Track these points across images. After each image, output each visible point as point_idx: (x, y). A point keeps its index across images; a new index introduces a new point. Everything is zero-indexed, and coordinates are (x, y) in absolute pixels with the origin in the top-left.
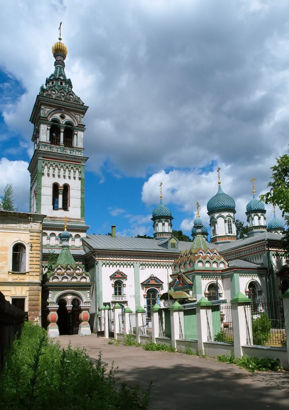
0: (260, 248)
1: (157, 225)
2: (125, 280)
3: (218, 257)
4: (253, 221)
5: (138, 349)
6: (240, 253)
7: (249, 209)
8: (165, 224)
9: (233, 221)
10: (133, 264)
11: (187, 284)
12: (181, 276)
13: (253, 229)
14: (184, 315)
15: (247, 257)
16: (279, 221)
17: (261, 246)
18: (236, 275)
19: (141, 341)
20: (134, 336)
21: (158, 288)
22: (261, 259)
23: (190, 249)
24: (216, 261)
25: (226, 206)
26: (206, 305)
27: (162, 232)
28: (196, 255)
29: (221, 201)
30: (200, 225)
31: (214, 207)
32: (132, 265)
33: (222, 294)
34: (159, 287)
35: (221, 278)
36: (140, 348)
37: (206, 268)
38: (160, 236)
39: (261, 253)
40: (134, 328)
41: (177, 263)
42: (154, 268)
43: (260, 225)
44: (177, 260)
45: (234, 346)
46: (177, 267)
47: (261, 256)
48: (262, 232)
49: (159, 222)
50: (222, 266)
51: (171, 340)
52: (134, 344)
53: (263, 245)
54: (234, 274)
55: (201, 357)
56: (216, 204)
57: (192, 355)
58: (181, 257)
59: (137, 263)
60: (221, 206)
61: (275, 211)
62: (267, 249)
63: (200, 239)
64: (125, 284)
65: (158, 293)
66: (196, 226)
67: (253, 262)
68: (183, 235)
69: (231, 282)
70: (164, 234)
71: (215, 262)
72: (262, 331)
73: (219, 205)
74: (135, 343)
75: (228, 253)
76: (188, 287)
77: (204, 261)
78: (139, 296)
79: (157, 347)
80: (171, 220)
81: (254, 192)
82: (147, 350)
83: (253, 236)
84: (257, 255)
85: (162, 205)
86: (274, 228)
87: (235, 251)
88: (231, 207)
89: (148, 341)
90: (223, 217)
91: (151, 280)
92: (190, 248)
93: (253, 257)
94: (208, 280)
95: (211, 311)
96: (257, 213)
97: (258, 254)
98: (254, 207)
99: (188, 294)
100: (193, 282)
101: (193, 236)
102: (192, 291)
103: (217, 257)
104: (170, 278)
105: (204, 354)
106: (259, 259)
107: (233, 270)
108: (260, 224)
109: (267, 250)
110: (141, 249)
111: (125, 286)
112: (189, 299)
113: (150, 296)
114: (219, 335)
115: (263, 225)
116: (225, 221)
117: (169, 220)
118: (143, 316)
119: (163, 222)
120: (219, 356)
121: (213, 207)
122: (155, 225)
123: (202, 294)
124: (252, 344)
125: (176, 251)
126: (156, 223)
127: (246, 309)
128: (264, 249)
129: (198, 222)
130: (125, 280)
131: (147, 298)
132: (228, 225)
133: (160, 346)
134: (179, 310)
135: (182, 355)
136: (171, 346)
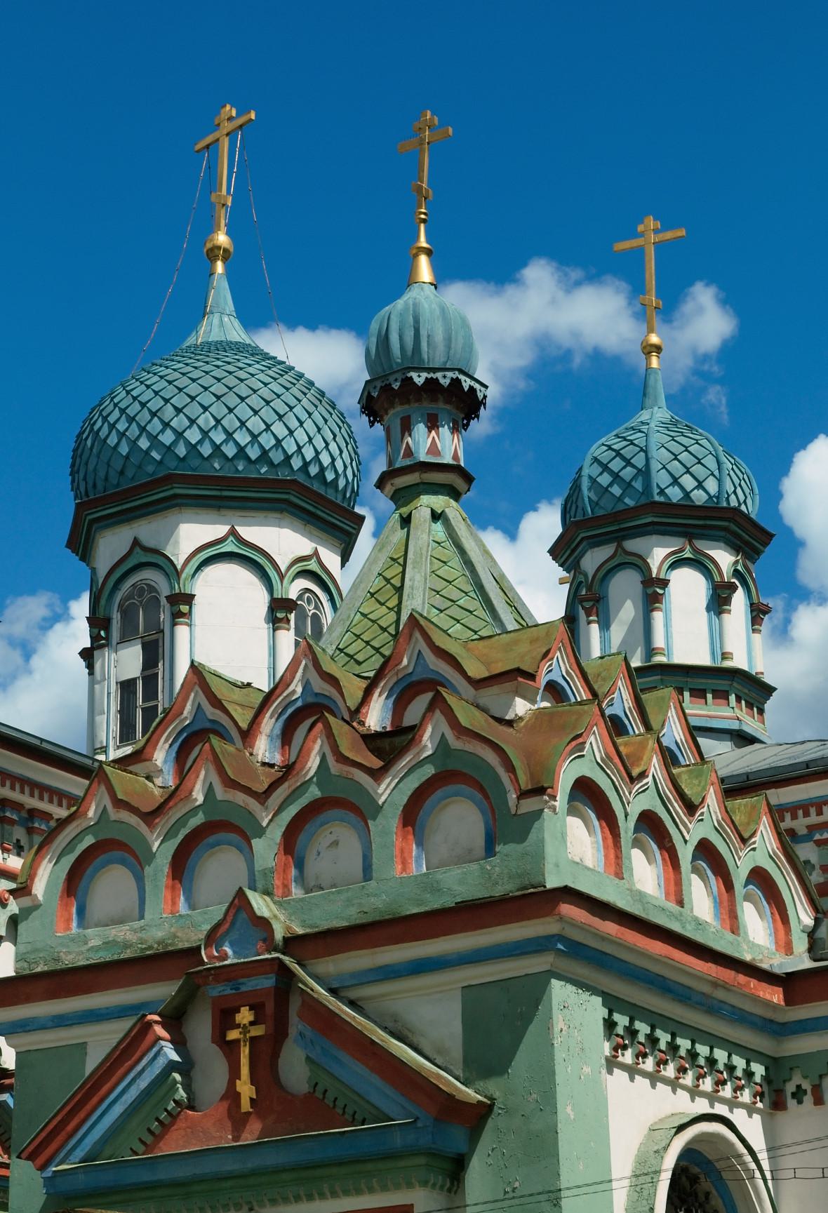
4: (658, 617)
25: (296, 463)
31: (181, 451)
43: (728, 664)
56: (206, 420)
60: (253, 453)
73: (229, 435)
81: (658, 349)
94: (654, 1078)
96: (699, 544)
98: (675, 481)
108: (725, 656)
116: (279, 610)
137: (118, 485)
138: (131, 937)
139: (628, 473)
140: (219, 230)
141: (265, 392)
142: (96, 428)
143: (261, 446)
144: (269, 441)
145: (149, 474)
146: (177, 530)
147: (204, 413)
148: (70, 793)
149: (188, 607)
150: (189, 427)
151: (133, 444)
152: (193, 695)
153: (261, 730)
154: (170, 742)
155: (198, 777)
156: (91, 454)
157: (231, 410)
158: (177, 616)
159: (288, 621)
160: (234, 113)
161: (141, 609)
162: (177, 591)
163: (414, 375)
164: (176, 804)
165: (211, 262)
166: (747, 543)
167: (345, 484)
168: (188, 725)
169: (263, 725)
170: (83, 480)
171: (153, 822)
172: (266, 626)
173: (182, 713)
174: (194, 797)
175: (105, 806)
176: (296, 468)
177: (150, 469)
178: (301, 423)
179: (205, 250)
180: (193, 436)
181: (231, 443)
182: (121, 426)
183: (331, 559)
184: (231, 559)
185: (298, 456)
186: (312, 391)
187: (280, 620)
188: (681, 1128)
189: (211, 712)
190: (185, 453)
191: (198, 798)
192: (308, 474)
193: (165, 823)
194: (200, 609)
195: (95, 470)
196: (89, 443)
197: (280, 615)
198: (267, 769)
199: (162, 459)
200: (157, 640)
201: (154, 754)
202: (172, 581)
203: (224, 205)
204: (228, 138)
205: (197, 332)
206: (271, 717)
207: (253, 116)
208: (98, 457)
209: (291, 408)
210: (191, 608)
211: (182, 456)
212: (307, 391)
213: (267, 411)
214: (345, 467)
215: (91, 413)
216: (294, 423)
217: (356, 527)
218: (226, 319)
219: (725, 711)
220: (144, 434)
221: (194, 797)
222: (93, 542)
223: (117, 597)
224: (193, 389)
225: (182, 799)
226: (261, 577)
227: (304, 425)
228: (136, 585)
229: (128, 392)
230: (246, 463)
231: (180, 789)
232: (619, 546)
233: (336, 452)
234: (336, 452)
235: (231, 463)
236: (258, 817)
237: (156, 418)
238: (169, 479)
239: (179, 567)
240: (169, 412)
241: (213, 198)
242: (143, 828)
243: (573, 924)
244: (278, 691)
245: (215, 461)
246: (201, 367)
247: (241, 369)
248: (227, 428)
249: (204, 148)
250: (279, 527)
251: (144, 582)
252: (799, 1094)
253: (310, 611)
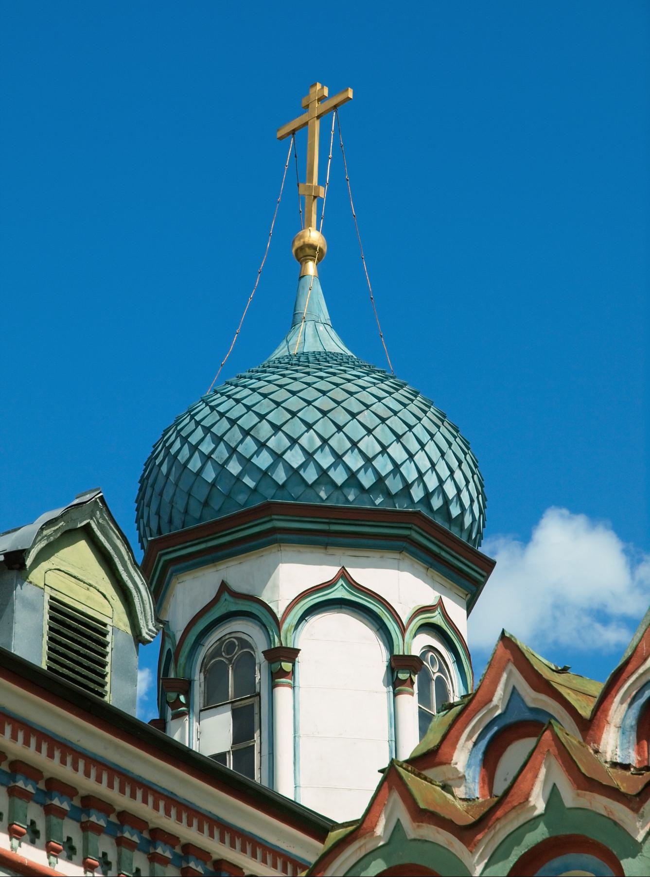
25: (417, 493)
31: (280, 476)
56: (310, 440)
73: (339, 458)
137: (201, 519)
140: (310, 226)
141: (378, 408)
142: (173, 451)
144: (385, 466)
145: (240, 505)
146: (276, 571)
147: (307, 431)
148: (266, 842)
149: (291, 664)
150: (290, 448)
151: (220, 469)
152: (505, 676)
153: (609, 719)
154: (474, 739)
155: (536, 776)
156: (166, 482)
157: (340, 428)
158: (277, 676)
159: (412, 683)
160: (326, 92)
161: (230, 668)
162: (277, 645)
164: (506, 814)
165: (301, 264)
167: (471, 522)
168: (499, 715)
169: (611, 712)
170: (156, 514)
171: (472, 840)
172: (385, 689)
173: (491, 700)
174: (532, 804)
175: (398, 820)
176: (416, 499)
177: (241, 498)
178: (423, 446)
179: (293, 250)
180: (295, 458)
181: (340, 468)
183: (456, 611)
184: (341, 608)
185: (418, 486)
186: (432, 409)
187: (403, 682)
189: (532, 698)
190: (285, 479)
191: (538, 805)
192: (429, 507)
193: (489, 841)
194: (304, 665)
195: (172, 502)
196: (164, 469)
197: (403, 676)
198: (620, 772)
199: (256, 486)
200: (252, 706)
201: (452, 756)
202: (271, 633)
203: (315, 197)
204: (319, 120)
205: (287, 342)
206: (622, 702)
207: (350, 94)
208: (176, 485)
209: (410, 427)
210: (294, 665)
211: (281, 483)
212: (427, 409)
213: (383, 430)
214: (472, 501)
215: (164, 436)
216: (414, 446)
217: (485, 574)
218: (321, 328)
220: (235, 456)
221: (532, 804)
222: (167, 588)
223: (199, 654)
224: (294, 403)
225: (514, 808)
226: (378, 630)
227: (426, 448)
228: (224, 639)
229: (213, 408)
230: (358, 493)
231: (510, 794)
233: (462, 483)
234: (462, 483)
235: (340, 492)
236: (629, 830)
237: (249, 437)
238: (267, 509)
239: (279, 616)
240: (265, 430)
241: (302, 190)
242: (457, 847)
244: (630, 667)
245: (321, 489)
246: (301, 378)
247: (349, 381)
248: (336, 450)
249: (288, 134)
250: (398, 570)
251: (233, 635)
253: (434, 673)
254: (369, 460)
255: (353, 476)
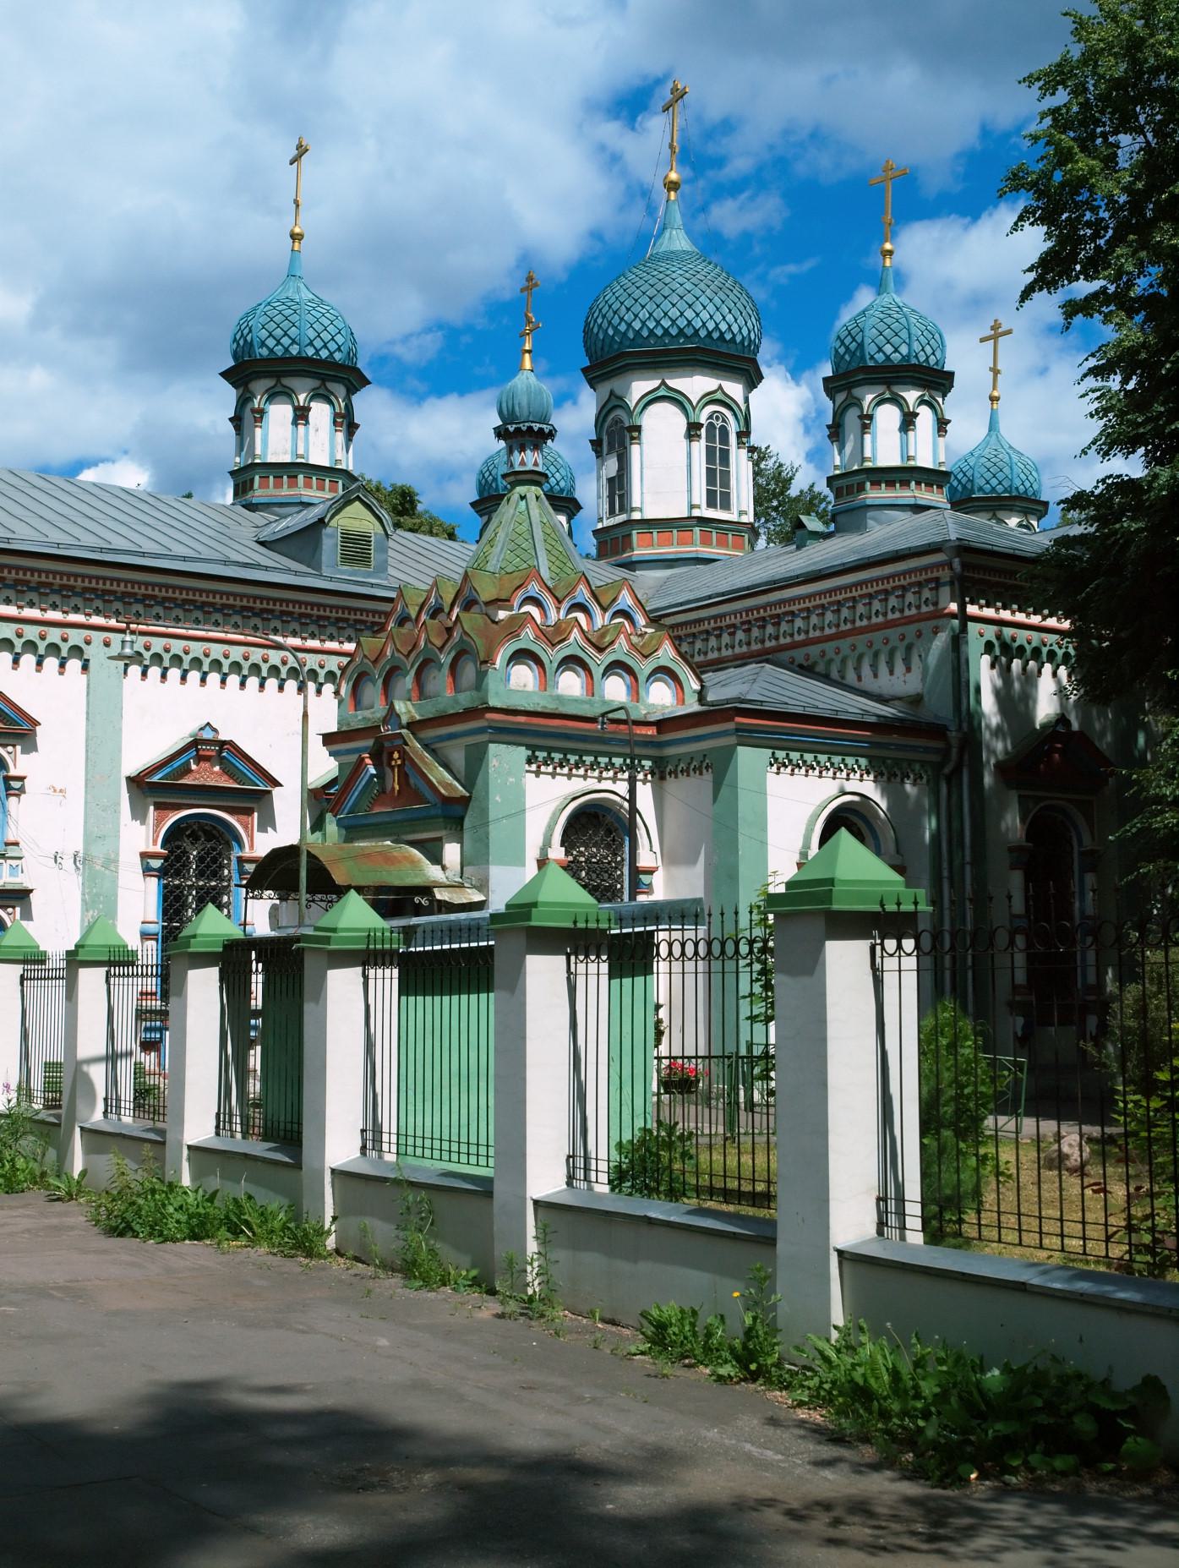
0: (910, 597)
1: (260, 414)
2: (19, 748)
3: (642, 635)
4: (867, 438)
5: (55, 1221)
6: (777, 620)
7: (847, 357)
8: (309, 409)
9: (739, 435)
10: (83, 646)
11: (428, 794)
12: (399, 742)
13: (861, 488)
14: (405, 989)
15: (823, 653)
16: (1015, 458)
17: (919, 584)
18: (749, 759)
19: (85, 1162)
20: (43, 1122)
21: (243, 818)
22: (909, 669)
23: (466, 577)
24: (630, 662)
25: (703, 333)
26: (570, 925)
27: (288, 460)
28: (502, 615)
29: (675, 298)
30: (536, 427)
32: (77, 651)
33: (650, 872)
34: (248, 812)
35: (653, 774)
36: (76, 1216)
37: (560, 699)
38: (271, 490)
39: (911, 630)
40: (49, 1066)
41: (375, 662)
42: (223, 682)
43: (912, 463)
44: (371, 643)
45: (780, 1245)
46: (370, 685)
47: (909, 648)
48: (918, 509)
49: (272, 396)
50: (660, 698)
51: (298, 1165)
52: (40, 1179)
53: (928, 581)
54: (739, 748)
55: (513, 1306)
56: (644, 314)
57: (448, 1290)
58: (403, 620)
59: (107, 644)
60: (674, 331)
61: (996, 394)
62: (954, 607)
63: (535, 512)
64: (21, 779)
65: (241, 846)
66: (511, 428)
67: (856, 684)
68: (419, 516)
69: (715, 799)
70: (301, 477)
71: (617, 666)
72: (954, 1125)
73: (658, 323)
74: (43, 1174)
75: (699, 621)
76: (436, 817)
77: (552, 656)
78: (112, 862)
79: (191, 1216)
80: (352, 390)
81: (890, 253)
82: (121, 1235)
83: (859, 527)
84: (887, 641)
85: (298, 291)
86: (981, 495)
87: (749, 610)
88: (733, 339)
89: (129, 1165)
90: (677, 399)
91: (200, 759)
92: (461, 571)
93: (857, 653)
95: (604, 967)
96: (895, 389)
97: (893, 634)
98: (880, 350)
99: (437, 859)
100: (469, 783)
101: (480, 513)
102: (461, 841)
103: (635, 639)
104: (317, 749)
105: (534, 1287)
106: (899, 667)
107: (730, 726)
108: (909, 458)
109: (953, 616)
110: (143, 555)
111: (22, 790)
112: (440, 895)
113: (186, 865)
114: (643, 1142)
115: (931, 466)
116: (693, 430)
117: (339, 390)
118: (115, 991)
119: (302, 397)
120: (655, 1313)
121: (625, 334)
122: (248, 415)
123: (524, 865)
124: (916, 1238)
125: (372, 585)
126: (256, 402)
127: (890, 964)
128: (936, 604)
129: (524, 403)
130: (19, 748)
131: (162, 873)
132: (710, 452)
133: (217, 1210)
134: (368, 957)
135: (370, 1284)
136: (296, 1212)
138: (370, 716)
139: (853, 346)
143: (678, 327)
157: (674, 305)
163: (509, 426)
166: (931, 382)
181: (659, 327)
182: (615, 307)
188: (575, 799)
219: (907, 493)
232: (849, 393)
243: (493, 720)
252: (670, 774)
254: (674, 322)
255: (666, 331)
